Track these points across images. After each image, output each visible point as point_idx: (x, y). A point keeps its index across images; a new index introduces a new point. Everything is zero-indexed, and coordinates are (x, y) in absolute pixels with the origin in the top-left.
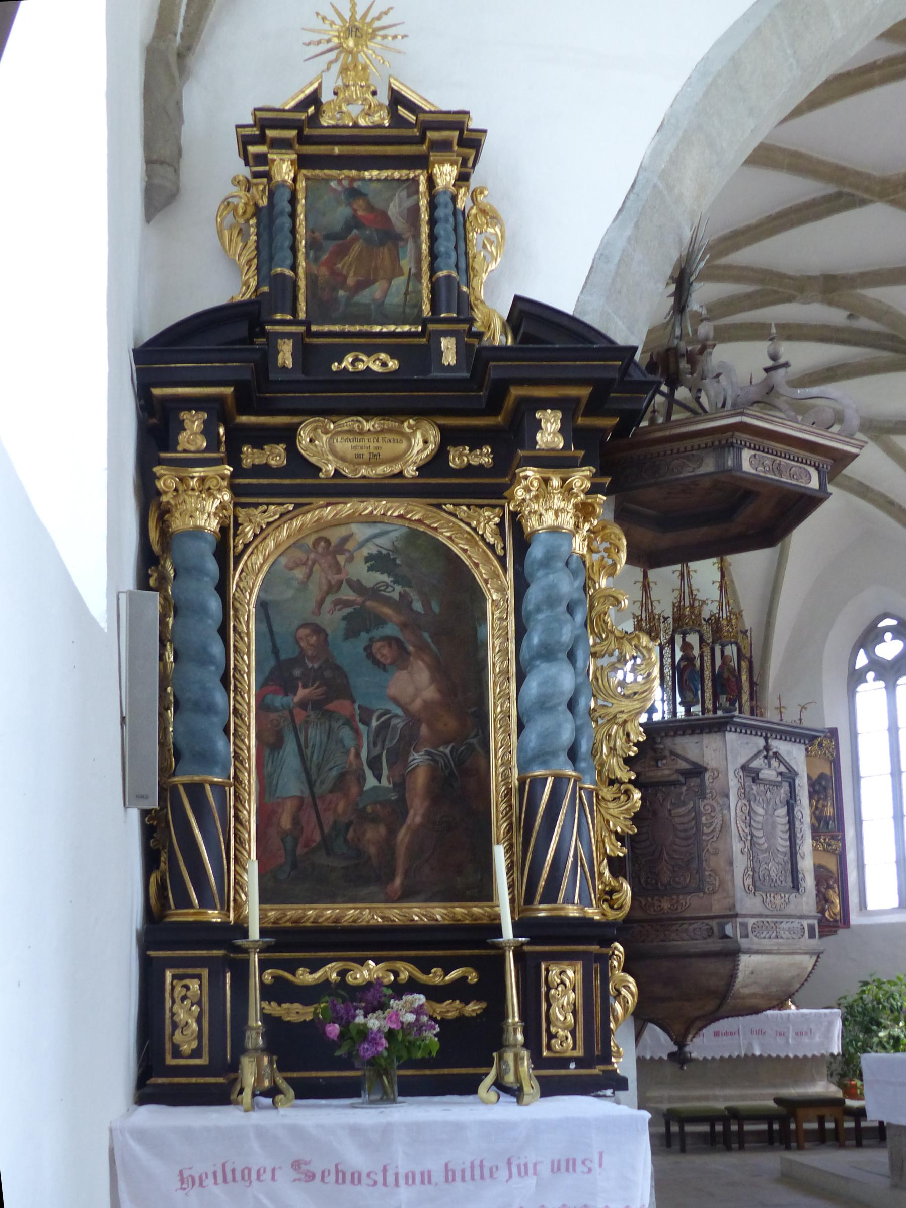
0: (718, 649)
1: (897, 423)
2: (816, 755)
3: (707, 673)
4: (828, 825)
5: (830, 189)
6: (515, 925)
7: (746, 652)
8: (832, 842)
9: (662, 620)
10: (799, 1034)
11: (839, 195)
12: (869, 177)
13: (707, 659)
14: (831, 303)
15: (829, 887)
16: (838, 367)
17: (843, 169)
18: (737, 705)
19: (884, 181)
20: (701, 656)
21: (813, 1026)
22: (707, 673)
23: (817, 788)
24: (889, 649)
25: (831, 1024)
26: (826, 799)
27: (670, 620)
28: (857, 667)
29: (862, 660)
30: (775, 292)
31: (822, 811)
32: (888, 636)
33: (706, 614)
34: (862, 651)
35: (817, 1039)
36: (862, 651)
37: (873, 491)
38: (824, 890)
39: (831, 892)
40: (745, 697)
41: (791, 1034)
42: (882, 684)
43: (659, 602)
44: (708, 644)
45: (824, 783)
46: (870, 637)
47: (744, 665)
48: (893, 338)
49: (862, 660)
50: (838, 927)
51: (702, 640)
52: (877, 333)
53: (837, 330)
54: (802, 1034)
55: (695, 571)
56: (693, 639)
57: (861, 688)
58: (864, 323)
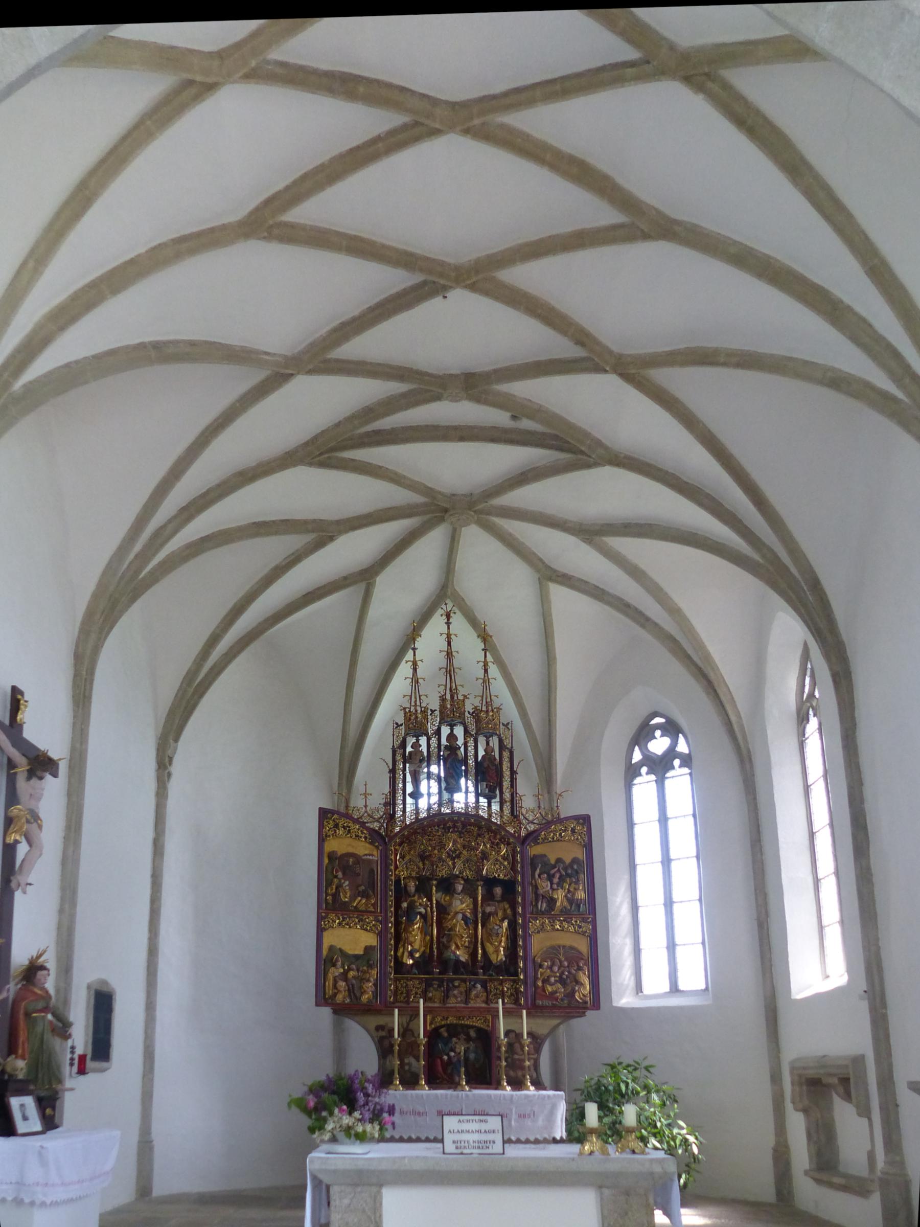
0: (482, 740)
1: (602, 525)
2: (569, 840)
3: (471, 762)
4: (579, 907)
5: (418, 278)
6: (528, 1034)
7: (506, 742)
8: (583, 924)
9: (429, 712)
10: (522, 1116)
11: (424, 283)
12: (442, 264)
13: (471, 749)
14: (478, 400)
15: (579, 969)
16: (529, 471)
17: (412, 255)
18: (498, 792)
19: (457, 268)
20: (465, 744)
21: (536, 1109)
22: (471, 762)
23: (570, 871)
24: (659, 745)
25: (554, 1107)
26: (577, 883)
27: (437, 713)
28: (634, 761)
29: (637, 756)
30: (427, 391)
31: (574, 894)
32: (658, 733)
33: (469, 707)
34: (637, 748)
35: (540, 1122)
36: (637, 748)
37: (609, 594)
38: (574, 972)
39: (581, 973)
40: (506, 784)
41: (514, 1116)
42: (653, 777)
43: (426, 696)
44: (472, 735)
45: (575, 867)
46: (643, 734)
47: (506, 754)
48: (556, 437)
49: (637, 756)
50: (587, 1008)
51: (466, 732)
52: (543, 434)
53: (505, 431)
54: (525, 1116)
55: (421, 661)
56: (459, 731)
57: (637, 780)
58: (526, 424)
